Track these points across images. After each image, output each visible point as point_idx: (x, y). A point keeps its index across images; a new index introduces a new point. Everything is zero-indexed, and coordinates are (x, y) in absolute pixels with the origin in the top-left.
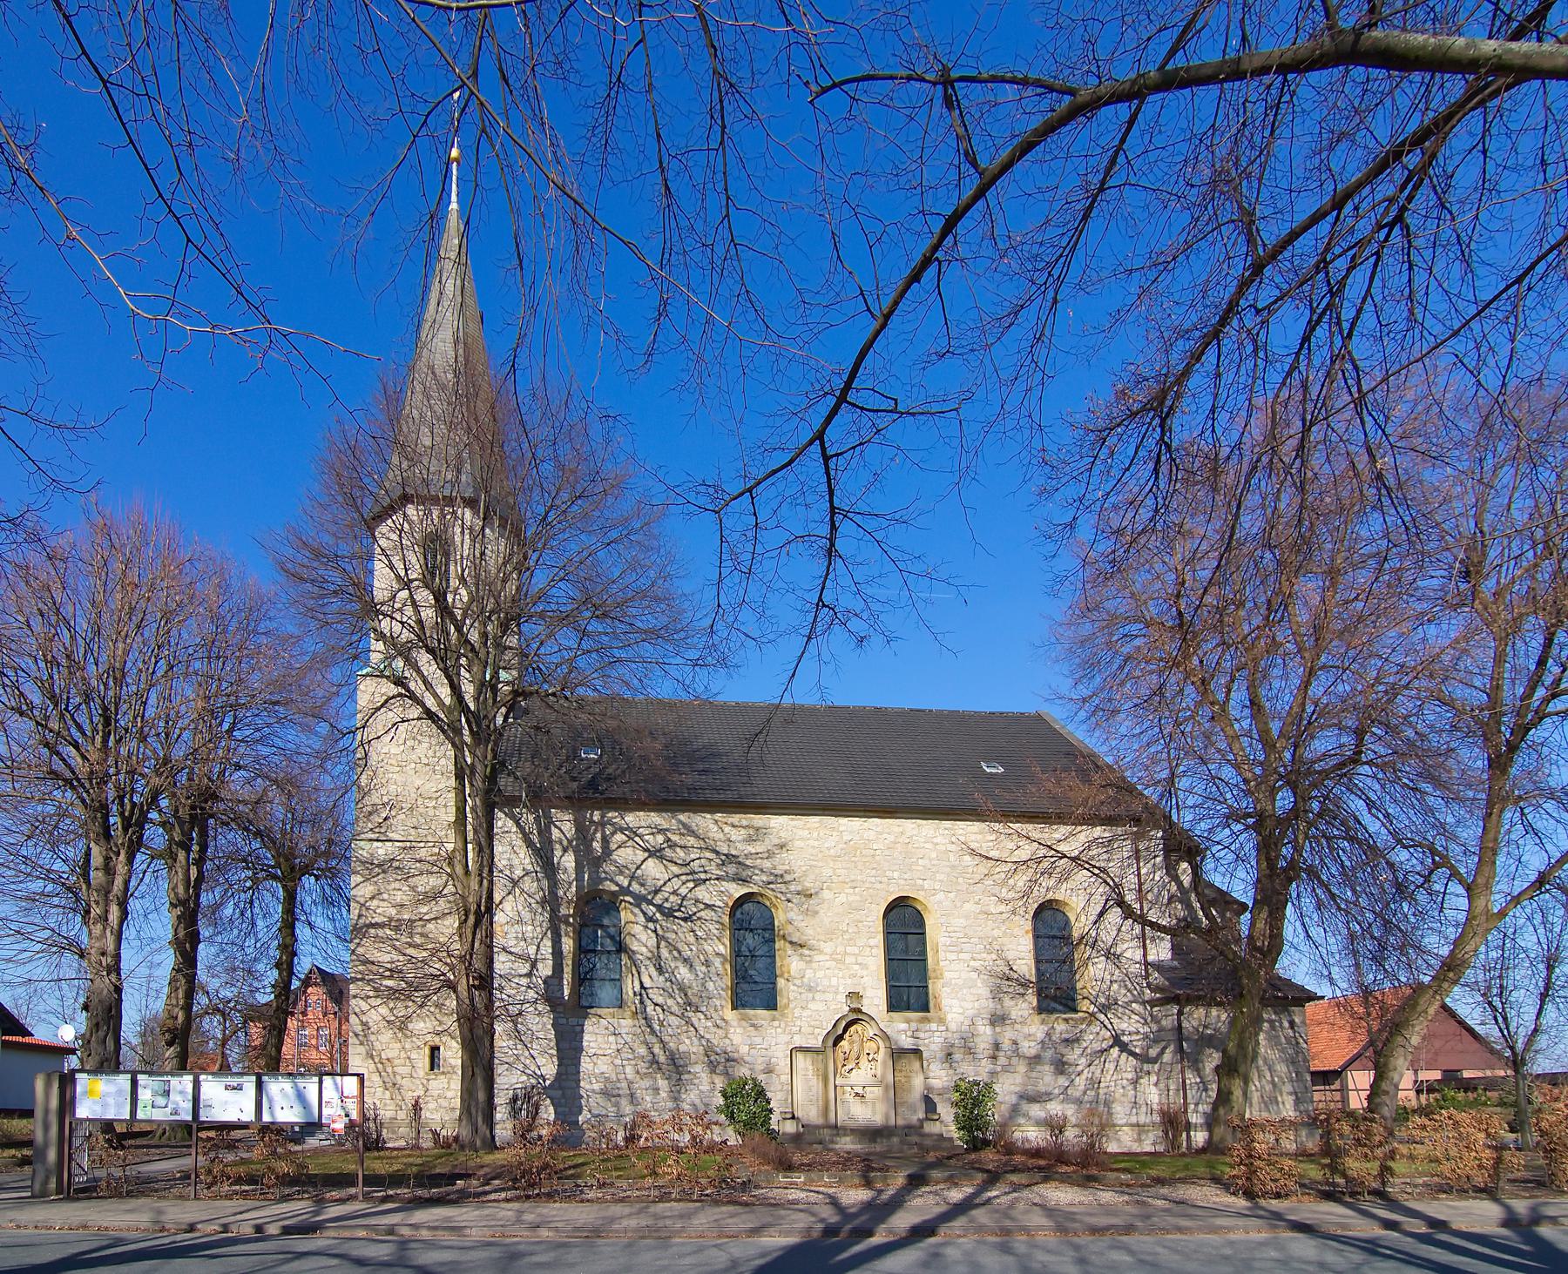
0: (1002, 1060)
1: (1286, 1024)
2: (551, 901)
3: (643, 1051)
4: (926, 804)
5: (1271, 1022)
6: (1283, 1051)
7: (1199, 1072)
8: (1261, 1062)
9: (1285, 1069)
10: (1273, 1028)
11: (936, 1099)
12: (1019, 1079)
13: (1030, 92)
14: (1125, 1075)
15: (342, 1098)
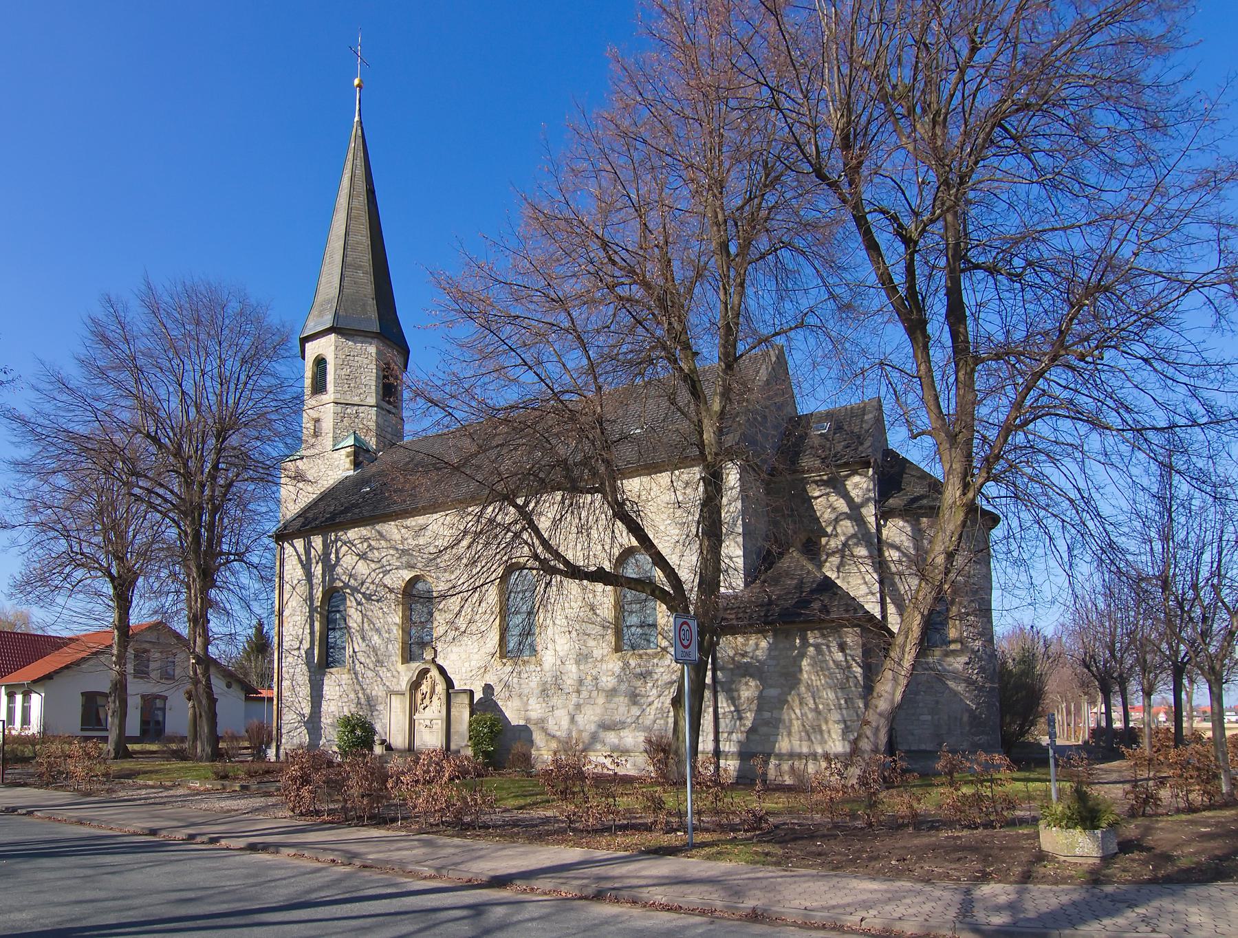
0: (584, 694)
1: (835, 649)
2: (311, 598)
3: (352, 696)
5: (817, 647)
6: (831, 676)
7: (733, 700)
8: (803, 689)
9: (831, 695)
12: (598, 710)
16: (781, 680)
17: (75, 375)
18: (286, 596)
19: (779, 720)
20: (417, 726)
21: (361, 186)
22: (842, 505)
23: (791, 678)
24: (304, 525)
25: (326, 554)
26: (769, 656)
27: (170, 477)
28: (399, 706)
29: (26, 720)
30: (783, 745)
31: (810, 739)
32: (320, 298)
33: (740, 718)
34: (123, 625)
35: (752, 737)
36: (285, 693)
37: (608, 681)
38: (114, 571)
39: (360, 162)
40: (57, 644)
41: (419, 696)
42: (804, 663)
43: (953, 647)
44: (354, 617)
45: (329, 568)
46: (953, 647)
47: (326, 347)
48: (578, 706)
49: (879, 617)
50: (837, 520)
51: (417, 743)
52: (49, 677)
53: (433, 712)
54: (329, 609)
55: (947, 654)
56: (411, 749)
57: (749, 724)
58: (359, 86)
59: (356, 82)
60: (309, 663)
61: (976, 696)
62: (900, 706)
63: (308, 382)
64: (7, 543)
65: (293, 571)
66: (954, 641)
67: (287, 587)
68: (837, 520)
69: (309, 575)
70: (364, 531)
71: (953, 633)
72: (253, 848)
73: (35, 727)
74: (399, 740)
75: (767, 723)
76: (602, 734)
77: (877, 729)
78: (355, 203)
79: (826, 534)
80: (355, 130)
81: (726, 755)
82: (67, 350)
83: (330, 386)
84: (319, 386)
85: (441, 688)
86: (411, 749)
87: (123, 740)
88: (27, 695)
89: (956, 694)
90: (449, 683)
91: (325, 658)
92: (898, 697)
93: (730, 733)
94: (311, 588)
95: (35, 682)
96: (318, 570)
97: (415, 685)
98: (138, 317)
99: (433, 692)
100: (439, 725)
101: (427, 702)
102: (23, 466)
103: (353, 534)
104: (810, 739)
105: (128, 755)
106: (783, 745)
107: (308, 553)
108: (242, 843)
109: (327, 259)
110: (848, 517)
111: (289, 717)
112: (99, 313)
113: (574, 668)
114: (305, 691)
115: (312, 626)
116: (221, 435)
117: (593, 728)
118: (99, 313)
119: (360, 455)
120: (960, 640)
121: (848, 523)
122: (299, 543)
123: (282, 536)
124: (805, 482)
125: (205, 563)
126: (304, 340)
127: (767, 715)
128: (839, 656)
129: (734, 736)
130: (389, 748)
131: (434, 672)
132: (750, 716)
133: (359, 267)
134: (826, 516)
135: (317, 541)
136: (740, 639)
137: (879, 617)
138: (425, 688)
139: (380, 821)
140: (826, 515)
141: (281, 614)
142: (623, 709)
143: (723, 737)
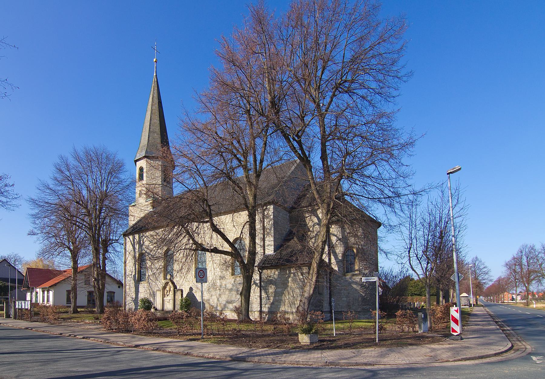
0: (222, 291)
1: (299, 274)
2: (135, 257)
3: (148, 291)
4: (473, 356)
5: (294, 273)
6: (298, 284)
7: (266, 293)
8: (289, 289)
9: (298, 291)
10: (294, 275)
11: (205, 302)
12: (226, 296)
13: (408, 241)
14: (256, 294)
15: (261, 312)
16: (282, 285)
17: (51, 184)
18: (127, 256)
19: (281, 300)
20: (166, 303)
21: (156, 101)
22: (316, 220)
23: (285, 285)
24: (133, 230)
25: (140, 241)
26: (278, 277)
27: (85, 216)
28: (159, 295)
29: (48, 301)
30: (282, 308)
31: (291, 307)
32: (141, 145)
33: (269, 299)
34: (75, 268)
35: (273, 306)
36: (127, 290)
37: (229, 286)
38: (72, 248)
39: (156, 91)
40: (60, 272)
41: (166, 292)
42: (290, 279)
43: (356, 272)
44: (149, 263)
45: (141, 246)
46: (356, 272)
47: (142, 163)
48: (220, 295)
49: (327, 261)
50: (314, 226)
51: (165, 308)
52: (55, 285)
53: (169, 298)
54: (141, 260)
55: (353, 275)
56: (163, 310)
57: (271, 301)
58: (156, 62)
59: (155, 60)
60: (134, 280)
61: (365, 291)
62: (312, 295)
63: (137, 176)
64: (36, 240)
65: (129, 247)
66: (357, 270)
67: (127, 253)
68: (314, 226)
69: (134, 248)
70: (152, 233)
71: (357, 267)
72: (84, 338)
73: (51, 302)
74: (159, 307)
75: (277, 301)
76: (227, 305)
77: (304, 303)
78: (154, 108)
79: (309, 231)
80: (154, 79)
81: (264, 312)
82: (48, 175)
83: (145, 178)
84: (141, 177)
85: (172, 289)
86: (163, 310)
87: (76, 307)
88: (48, 291)
89: (356, 290)
90: (175, 287)
91: (140, 278)
92: (311, 292)
93: (266, 304)
94: (135, 253)
95: (50, 287)
96: (137, 247)
97: (164, 288)
98: (72, 162)
99: (170, 290)
100: (172, 302)
101: (168, 293)
102: (35, 216)
103: (147, 234)
104: (291, 307)
105: (78, 312)
106: (282, 308)
107: (134, 240)
108: (82, 337)
109: (144, 130)
110: (318, 224)
111: (129, 299)
112: (58, 161)
113: (218, 281)
114: (133, 289)
115: (135, 266)
116: (102, 201)
117: (224, 303)
118: (58, 161)
119: (155, 203)
120: (359, 270)
121: (317, 226)
122: (131, 237)
123: (126, 235)
124: (303, 212)
125: (102, 245)
126: (136, 161)
127: (277, 298)
128: (301, 277)
129: (267, 306)
130: (156, 309)
131: (170, 284)
132: (272, 298)
133: (155, 132)
134: (310, 224)
135: (137, 236)
136: (269, 271)
137: (327, 261)
138: (168, 289)
139: (128, 331)
140: (310, 224)
141: (125, 262)
142: (234, 296)
143: (263, 306)
